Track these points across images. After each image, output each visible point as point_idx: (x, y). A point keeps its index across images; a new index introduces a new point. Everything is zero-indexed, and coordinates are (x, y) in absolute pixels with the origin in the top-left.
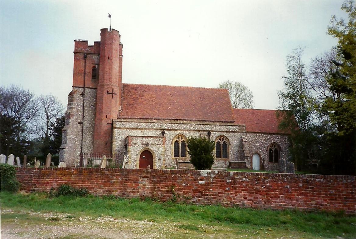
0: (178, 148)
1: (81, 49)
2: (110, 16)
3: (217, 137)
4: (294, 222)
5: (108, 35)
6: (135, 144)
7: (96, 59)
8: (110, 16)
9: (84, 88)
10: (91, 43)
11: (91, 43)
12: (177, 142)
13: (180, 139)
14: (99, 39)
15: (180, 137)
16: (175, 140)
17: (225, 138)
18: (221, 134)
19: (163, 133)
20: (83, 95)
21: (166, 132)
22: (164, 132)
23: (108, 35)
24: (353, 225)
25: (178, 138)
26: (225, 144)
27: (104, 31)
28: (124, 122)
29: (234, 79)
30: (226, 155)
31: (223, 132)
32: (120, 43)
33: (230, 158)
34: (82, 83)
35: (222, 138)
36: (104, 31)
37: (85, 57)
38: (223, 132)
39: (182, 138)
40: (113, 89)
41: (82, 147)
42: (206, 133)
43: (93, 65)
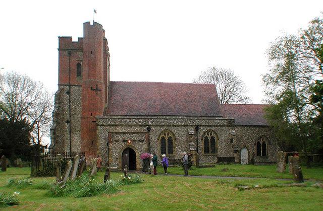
0: (165, 145)
1: (65, 43)
2: (95, 11)
3: (205, 133)
4: (318, 45)
5: (94, 31)
6: (116, 141)
7: (82, 56)
8: (95, 11)
9: (70, 86)
10: (75, 39)
11: (75, 39)
12: (163, 139)
13: (166, 135)
14: (82, 36)
15: (166, 133)
16: (162, 136)
17: (213, 133)
18: (208, 128)
19: (149, 129)
20: (69, 93)
21: (153, 128)
22: (150, 128)
23: (94, 31)
24: (54, 132)
25: (165, 134)
26: (213, 138)
27: (87, 25)
28: (107, 118)
29: (223, 65)
30: (214, 150)
31: (211, 126)
32: (104, 37)
33: (219, 153)
34: (68, 82)
35: (210, 133)
36: (87, 25)
37: (70, 54)
38: (211, 126)
39: (168, 134)
40: (97, 85)
41: (70, 147)
42: (194, 128)
43: (77, 62)
